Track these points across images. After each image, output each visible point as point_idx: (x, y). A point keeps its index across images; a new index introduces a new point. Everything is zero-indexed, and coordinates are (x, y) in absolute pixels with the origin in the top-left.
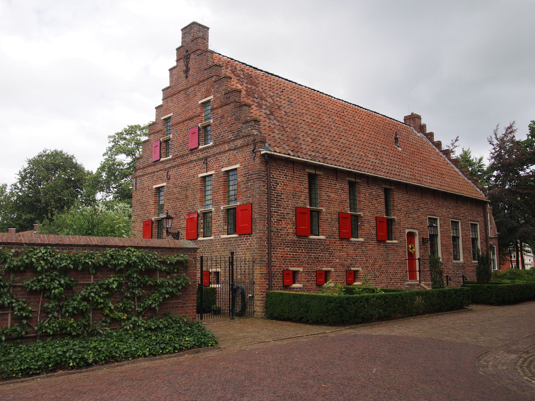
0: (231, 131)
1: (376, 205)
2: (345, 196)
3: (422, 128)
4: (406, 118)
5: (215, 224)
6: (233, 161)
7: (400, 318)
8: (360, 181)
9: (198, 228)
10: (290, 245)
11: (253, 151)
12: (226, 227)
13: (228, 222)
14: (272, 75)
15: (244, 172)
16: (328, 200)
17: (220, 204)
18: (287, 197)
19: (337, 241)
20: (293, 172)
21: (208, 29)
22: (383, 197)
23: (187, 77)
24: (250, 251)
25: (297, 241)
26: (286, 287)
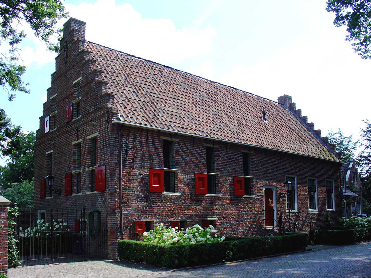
0: (93, 105)
1: (235, 167)
2: (203, 160)
3: (292, 106)
4: (280, 99)
5: (83, 182)
6: (94, 130)
7: (141, 268)
8: (218, 147)
9: (72, 186)
10: (156, 201)
11: (107, 121)
12: (90, 185)
13: (92, 181)
14: (150, 61)
15: (101, 139)
16: (184, 163)
17: (86, 167)
18: (140, 160)
19: (193, 196)
20: (147, 139)
21: (85, 23)
22: (241, 160)
23: (66, 63)
24: (105, 205)
25: (151, 196)
26: (136, 235)
